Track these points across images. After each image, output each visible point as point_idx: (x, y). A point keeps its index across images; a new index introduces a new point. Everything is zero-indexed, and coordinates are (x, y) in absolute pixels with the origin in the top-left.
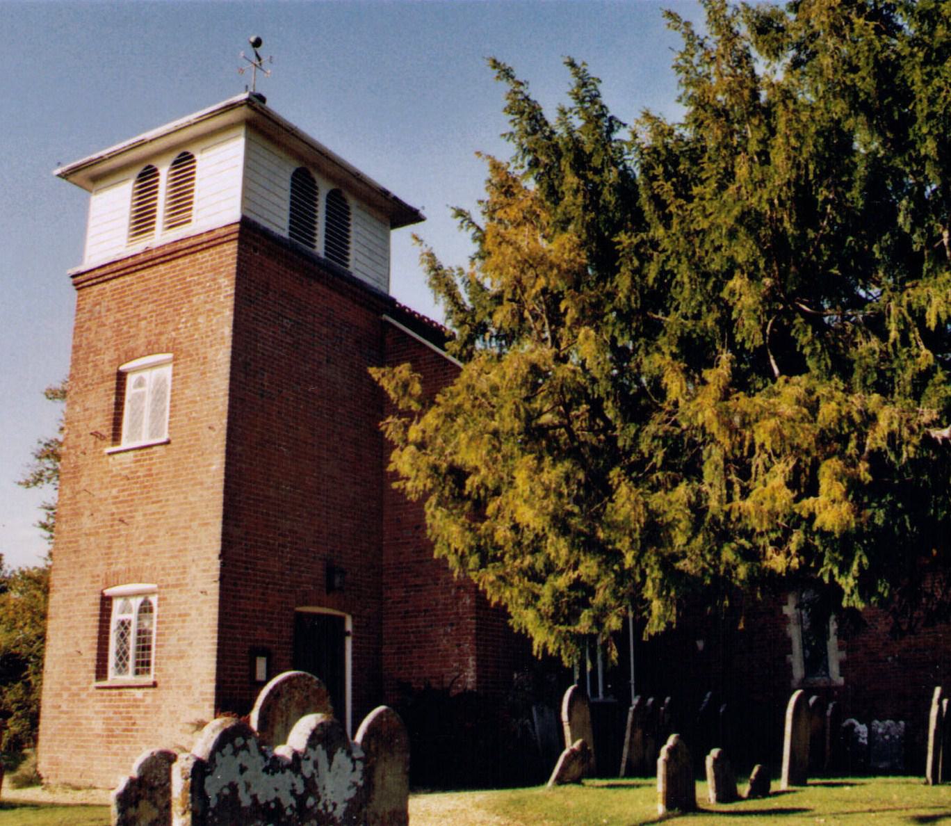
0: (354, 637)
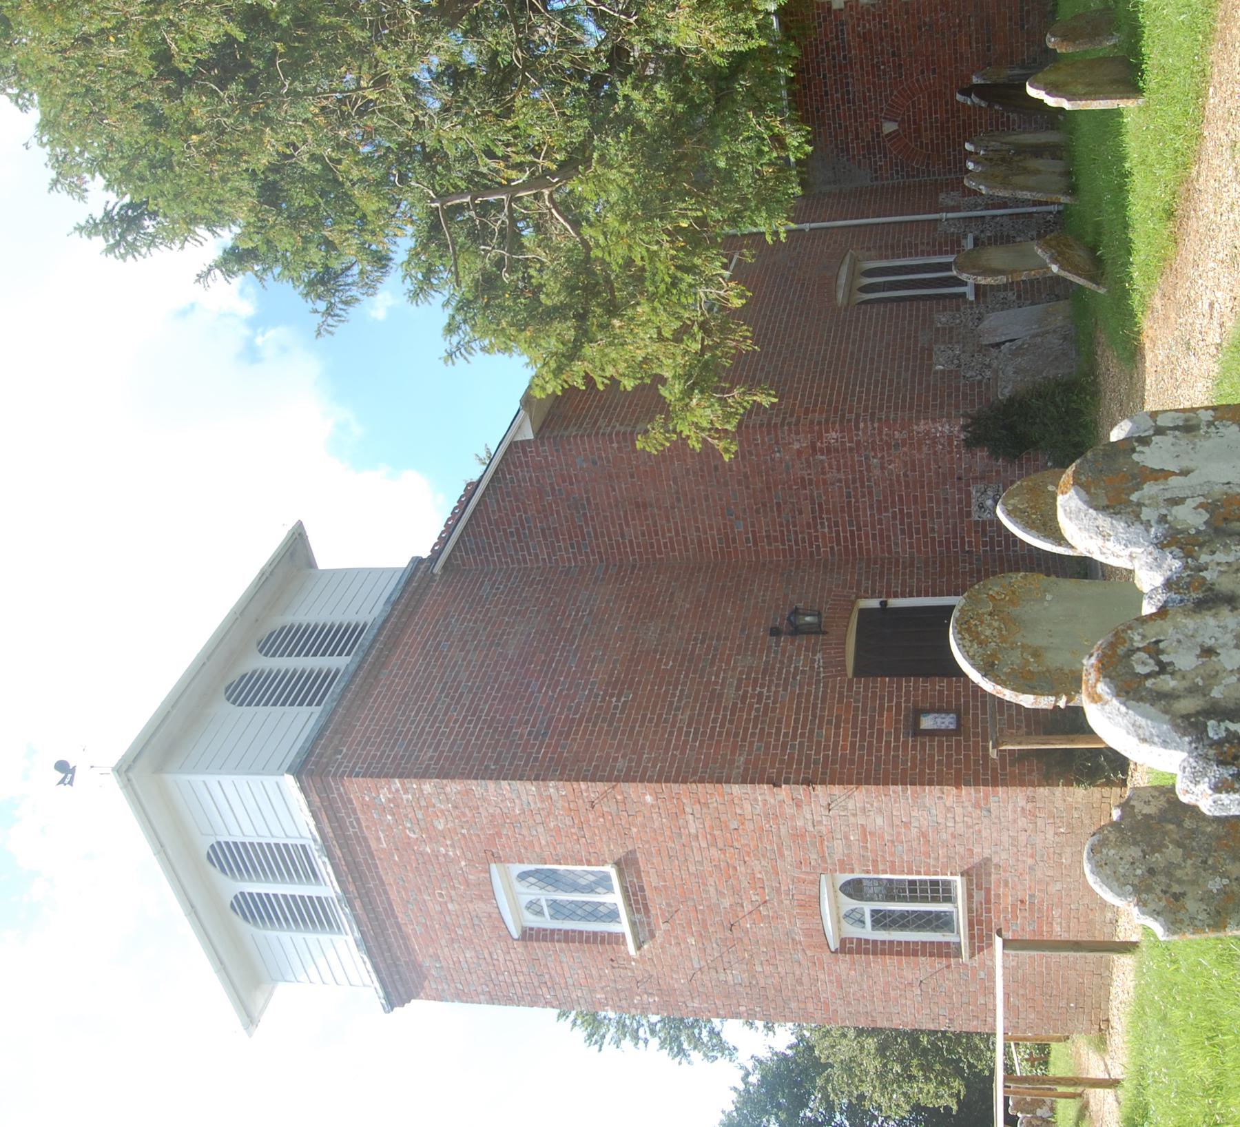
0: (889, 596)
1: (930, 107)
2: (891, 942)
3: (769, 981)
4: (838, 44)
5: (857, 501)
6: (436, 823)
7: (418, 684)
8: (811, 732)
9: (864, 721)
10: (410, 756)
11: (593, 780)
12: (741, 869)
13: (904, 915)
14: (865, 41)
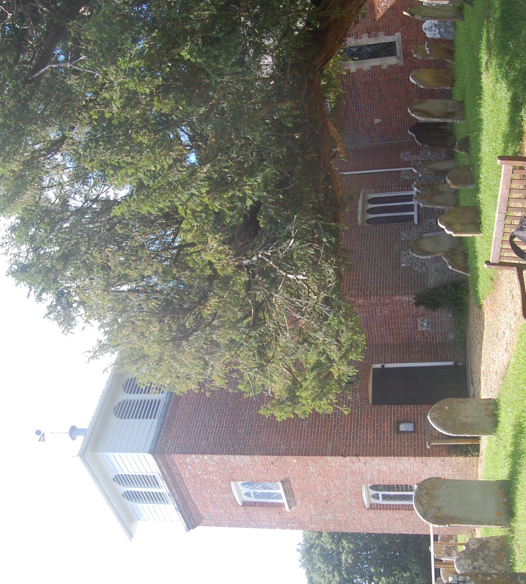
0: (385, 363)
1: (396, 113)
2: (390, 505)
3: (342, 519)
4: (353, 87)
5: (371, 324)
6: (209, 469)
7: (195, 408)
8: (357, 431)
9: (377, 426)
10: (197, 444)
11: (272, 455)
12: (331, 483)
13: (394, 496)
14: (366, 85)
